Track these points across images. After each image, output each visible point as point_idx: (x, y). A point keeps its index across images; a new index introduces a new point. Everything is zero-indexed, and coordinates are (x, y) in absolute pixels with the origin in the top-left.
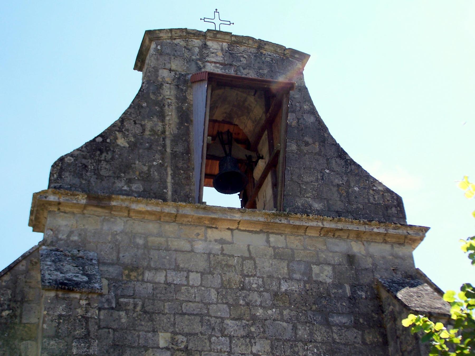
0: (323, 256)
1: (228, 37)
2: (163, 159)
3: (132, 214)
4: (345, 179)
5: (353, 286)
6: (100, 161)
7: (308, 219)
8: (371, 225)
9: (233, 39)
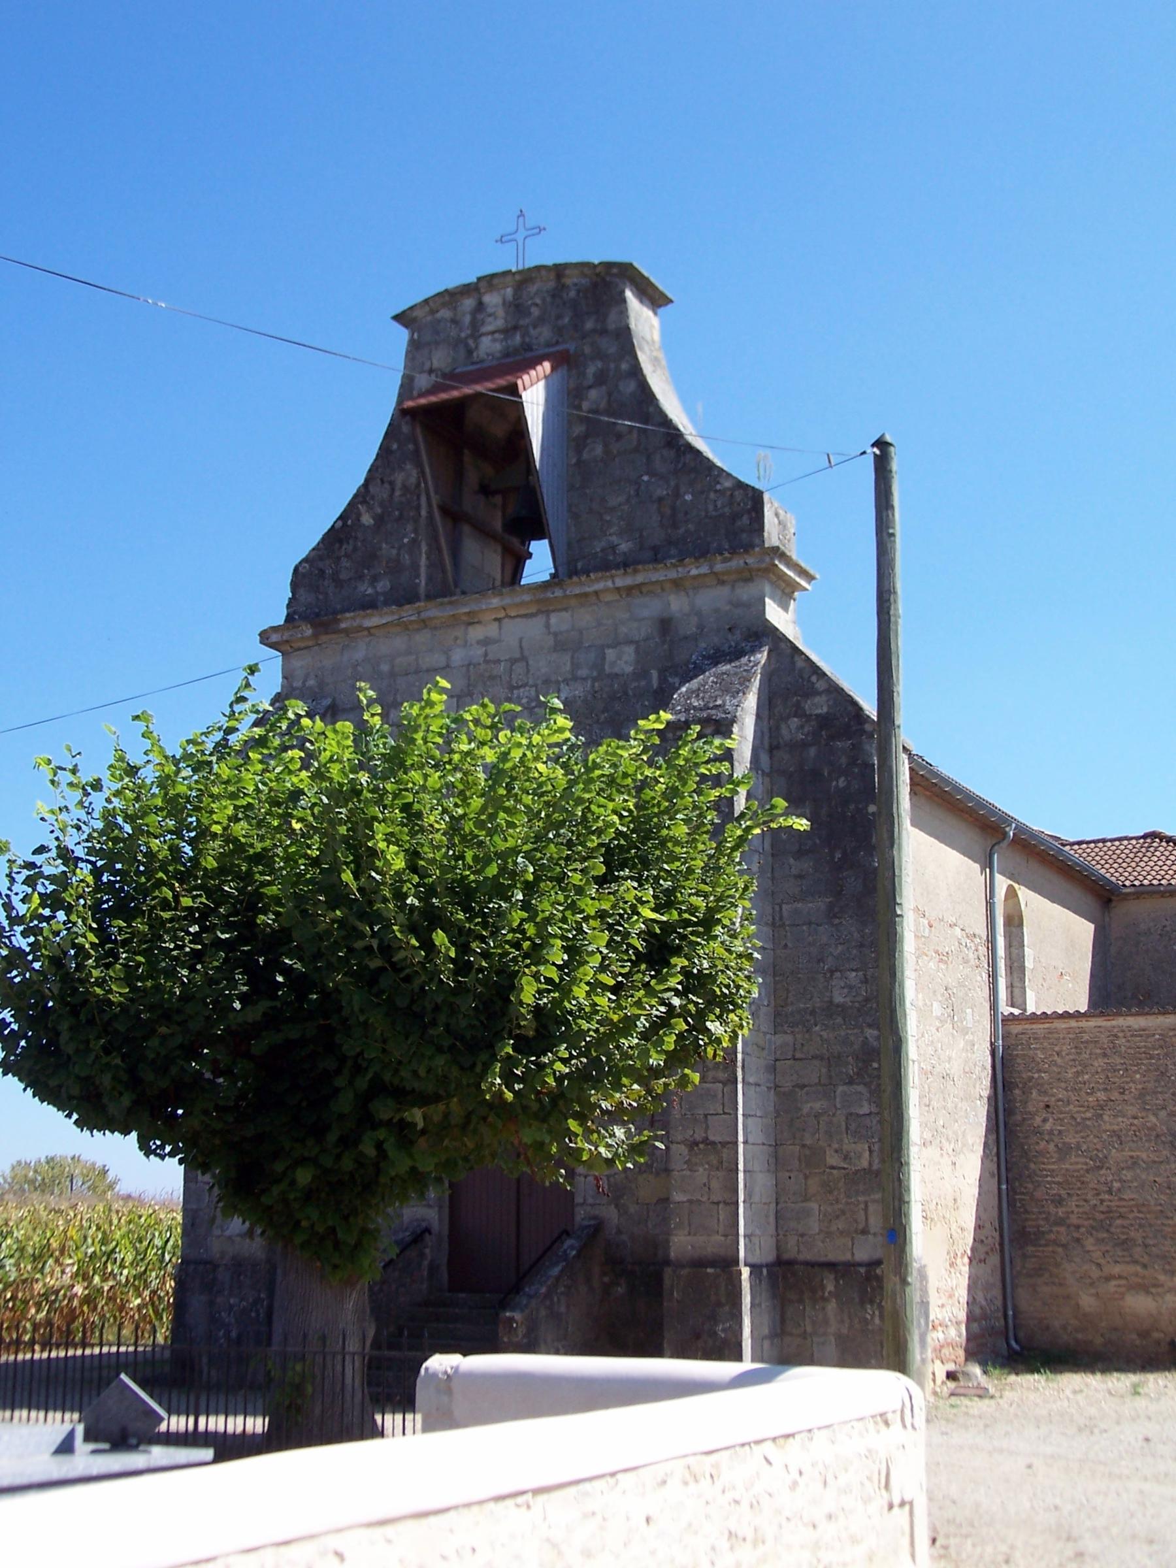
0: (623, 630)
1: (509, 279)
2: (416, 531)
3: (372, 631)
4: (672, 483)
5: (663, 673)
6: (339, 558)
7: (592, 581)
8: (684, 566)
9: (518, 277)
